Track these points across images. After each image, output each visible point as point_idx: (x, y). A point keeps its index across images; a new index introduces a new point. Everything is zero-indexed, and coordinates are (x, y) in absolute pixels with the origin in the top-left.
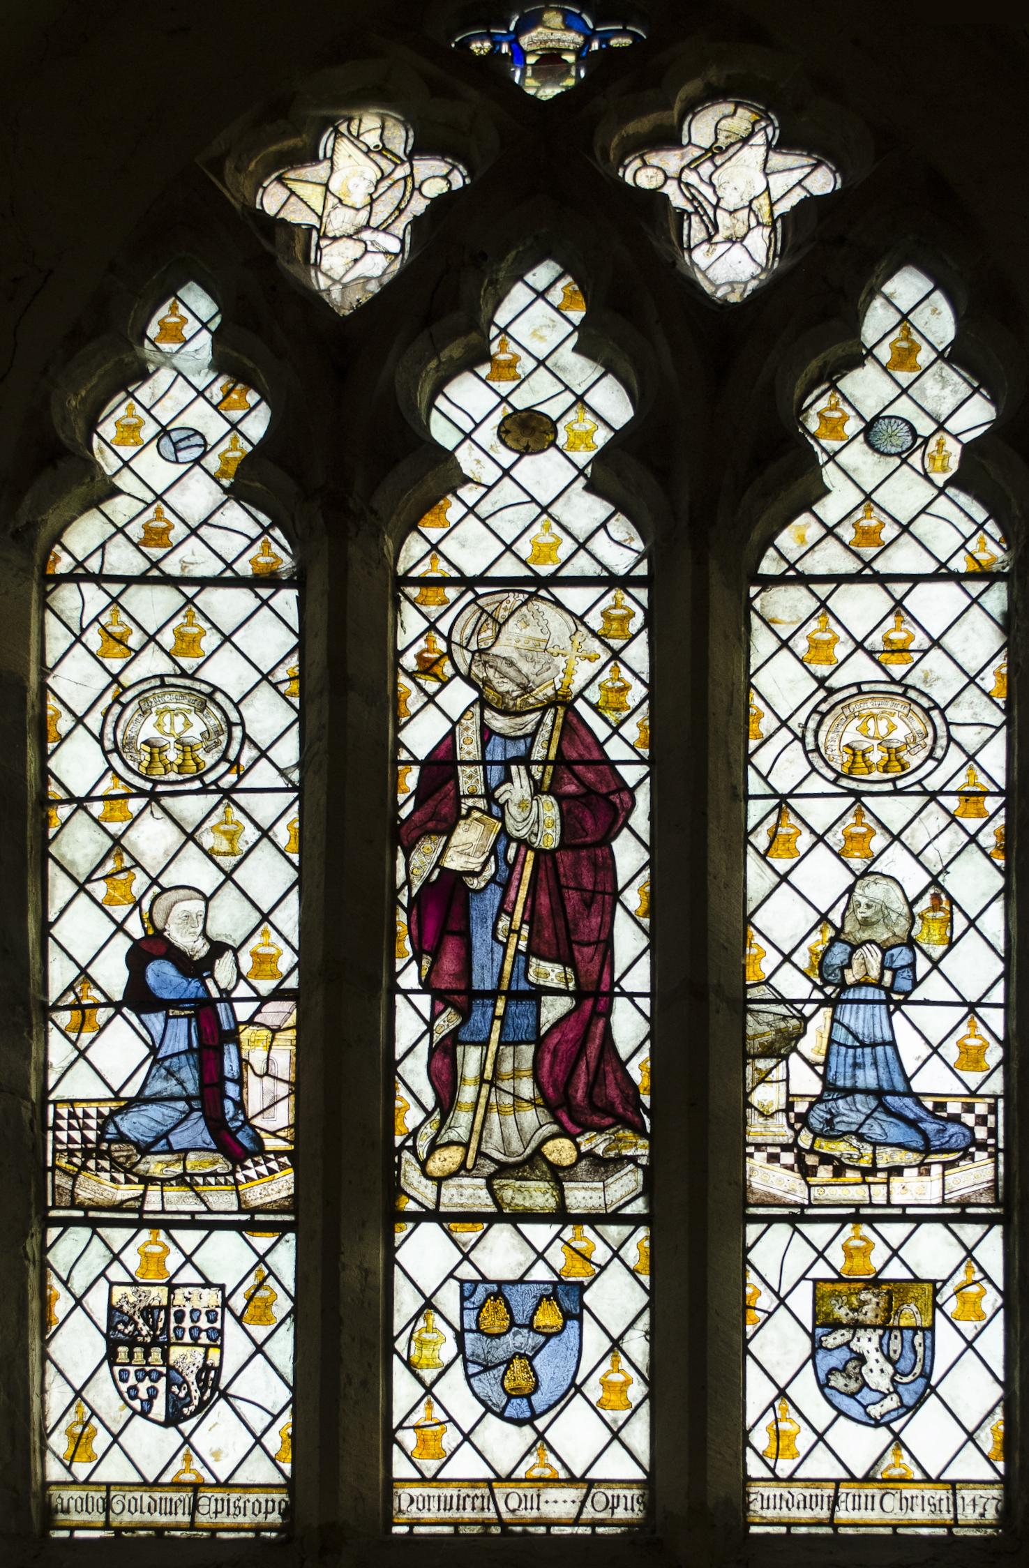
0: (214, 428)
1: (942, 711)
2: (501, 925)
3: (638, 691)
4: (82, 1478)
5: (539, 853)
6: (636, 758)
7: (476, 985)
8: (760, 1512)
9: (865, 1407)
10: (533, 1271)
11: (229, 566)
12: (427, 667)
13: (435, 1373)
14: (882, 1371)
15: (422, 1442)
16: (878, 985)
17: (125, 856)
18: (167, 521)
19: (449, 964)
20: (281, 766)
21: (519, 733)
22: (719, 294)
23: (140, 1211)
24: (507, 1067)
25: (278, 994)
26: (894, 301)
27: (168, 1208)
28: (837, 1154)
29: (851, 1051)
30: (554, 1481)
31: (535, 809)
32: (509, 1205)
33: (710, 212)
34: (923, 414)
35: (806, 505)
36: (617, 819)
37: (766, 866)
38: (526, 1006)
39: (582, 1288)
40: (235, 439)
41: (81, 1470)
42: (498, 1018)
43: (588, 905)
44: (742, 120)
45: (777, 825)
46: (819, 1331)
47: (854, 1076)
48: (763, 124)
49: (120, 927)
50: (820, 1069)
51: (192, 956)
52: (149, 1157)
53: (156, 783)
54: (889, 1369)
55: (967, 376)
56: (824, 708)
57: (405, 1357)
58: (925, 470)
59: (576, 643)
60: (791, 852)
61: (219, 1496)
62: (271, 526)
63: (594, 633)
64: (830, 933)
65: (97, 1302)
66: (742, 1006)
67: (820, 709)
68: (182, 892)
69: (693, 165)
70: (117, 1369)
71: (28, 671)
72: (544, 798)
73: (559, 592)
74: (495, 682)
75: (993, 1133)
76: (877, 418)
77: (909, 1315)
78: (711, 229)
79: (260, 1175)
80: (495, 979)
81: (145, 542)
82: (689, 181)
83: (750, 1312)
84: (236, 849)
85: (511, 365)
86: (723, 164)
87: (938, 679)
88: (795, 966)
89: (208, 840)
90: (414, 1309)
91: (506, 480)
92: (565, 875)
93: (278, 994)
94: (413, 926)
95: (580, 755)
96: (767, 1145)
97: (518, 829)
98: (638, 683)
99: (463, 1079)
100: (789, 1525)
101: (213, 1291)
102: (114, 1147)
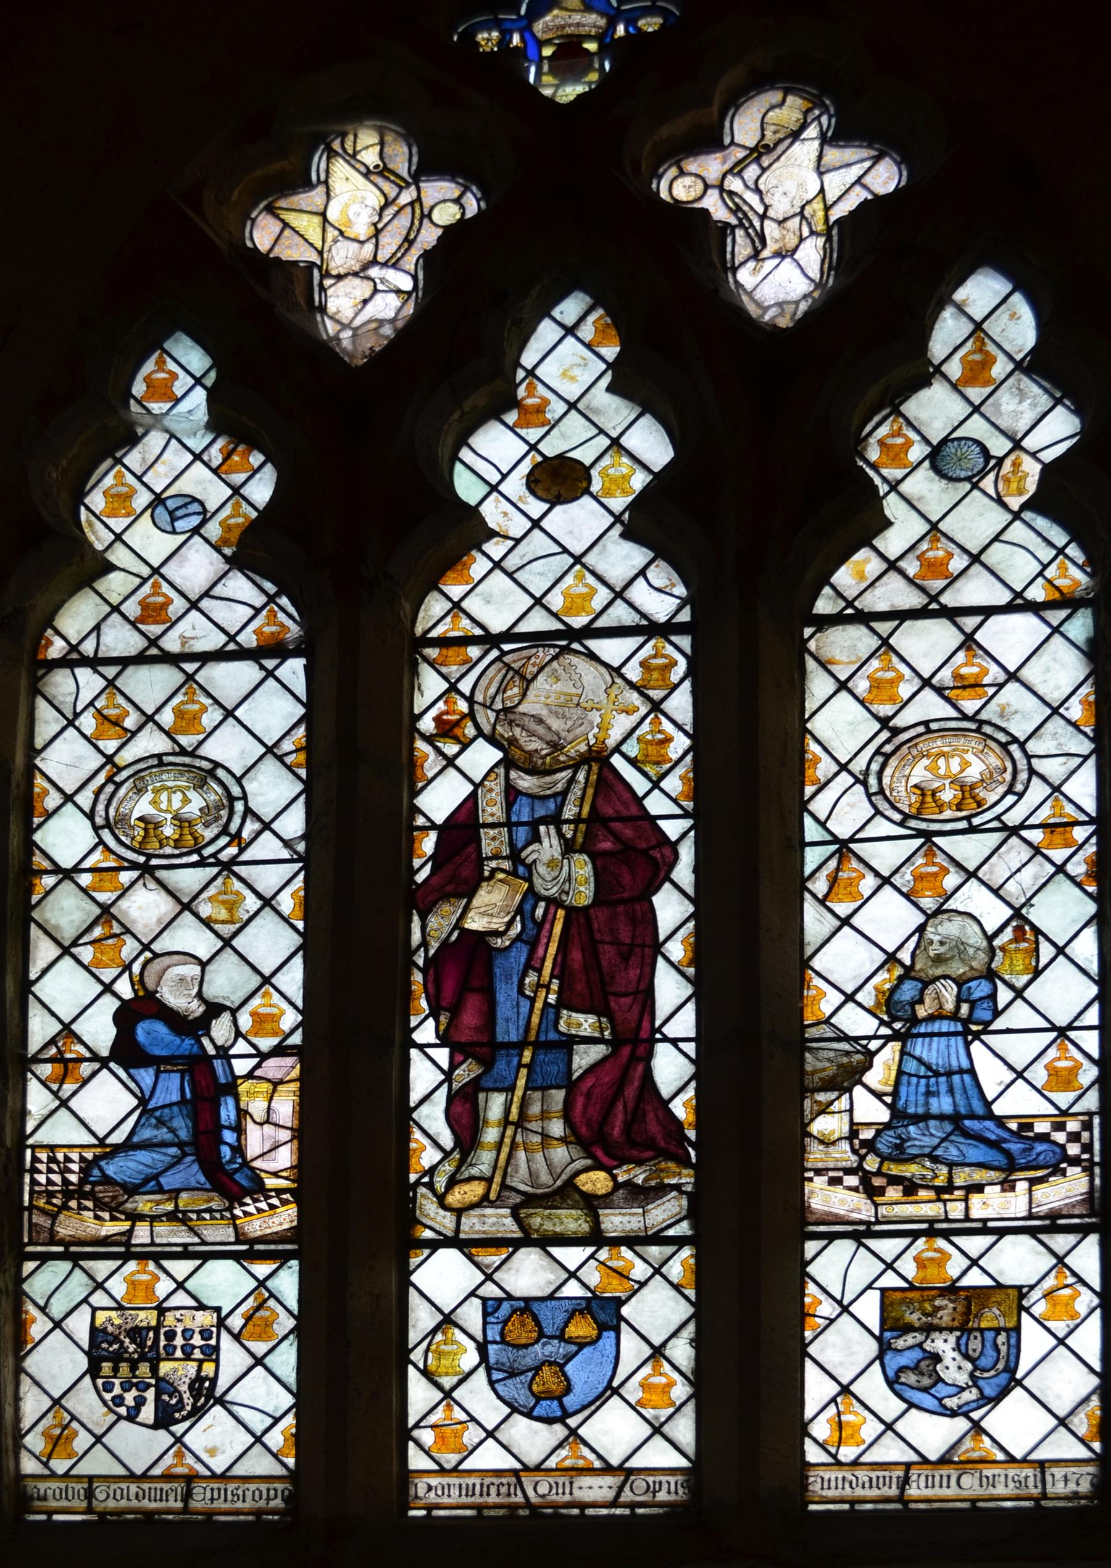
0: (215, 493)
1: (1022, 745)
2: (527, 981)
3: (680, 743)
4: (60, 1472)
5: (571, 911)
6: (679, 812)
7: (500, 1037)
8: (820, 1492)
9: (940, 1400)
10: (564, 1289)
11: (232, 638)
12: (446, 729)
13: (455, 1380)
14: (960, 1368)
15: (441, 1439)
16: (954, 1016)
17: (114, 923)
18: (165, 595)
19: (470, 1018)
20: (286, 837)
21: (548, 792)
22: (767, 318)
23: (128, 1244)
24: (535, 1109)
25: (279, 1051)
26: (968, 310)
27: (158, 1241)
28: (908, 1175)
29: (923, 1081)
30: (589, 1471)
31: (566, 868)
32: (537, 1231)
33: (757, 224)
34: (997, 433)
35: (866, 541)
36: (659, 872)
37: (825, 911)
38: (559, 1055)
39: (620, 1302)
40: (237, 505)
41: (60, 1466)
42: (525, 1066)
43: (626, 958)
44: (791, 111)
45: (838, 869)
46: (887, 1335)
47: (927, 1104)
48: (817, 112)
49: (108, 989)
50: (888, 1100)
51: (186, 1016)
52: (137, 1197)
53: (149, 857)
54: (969, 1366)
55: (1048, 386)
56: (888, 748)
57: (421, 1366)
58: (998, 493)
59: (613, 696)
60: (853, 896)
61: (215, 1486)
62: (278, 594)
63: (631, 685)
64: (898, 971)
65: (80, 1325)
66: (800, 1045)
67: (884, 750)
68: (176, 957)
69: (737, 169)
70: (100, 1382)
71: (14, 753)
72: (576, 856)
73: (594, 645)
74: (522, 741)
75: (1087, 1148)
76: (945, 441)
77: (991, 1318)
78: (758, 244)
79: (260, 1211)
80: (521, 1031)
81: (142, 619)
82: (732, 188)
83: (809, 1320)
84: (236, 918)
85: (540, 409)
86: (770, 165)
87: (1016, 712)
88: (859, 1005)
89: (205, 910)
90: (432, 1325)
91: (536, 532)
92: (600, 931)
93: (279, 1051)
94: (429, 985)
95: (617, 812)
96: (828, 1170)
97: (546, 886)
98: (681, 734)
99: (486, 1122)
100: (852, 1502)
101: (207, 1313)
102: (98, 1188)
